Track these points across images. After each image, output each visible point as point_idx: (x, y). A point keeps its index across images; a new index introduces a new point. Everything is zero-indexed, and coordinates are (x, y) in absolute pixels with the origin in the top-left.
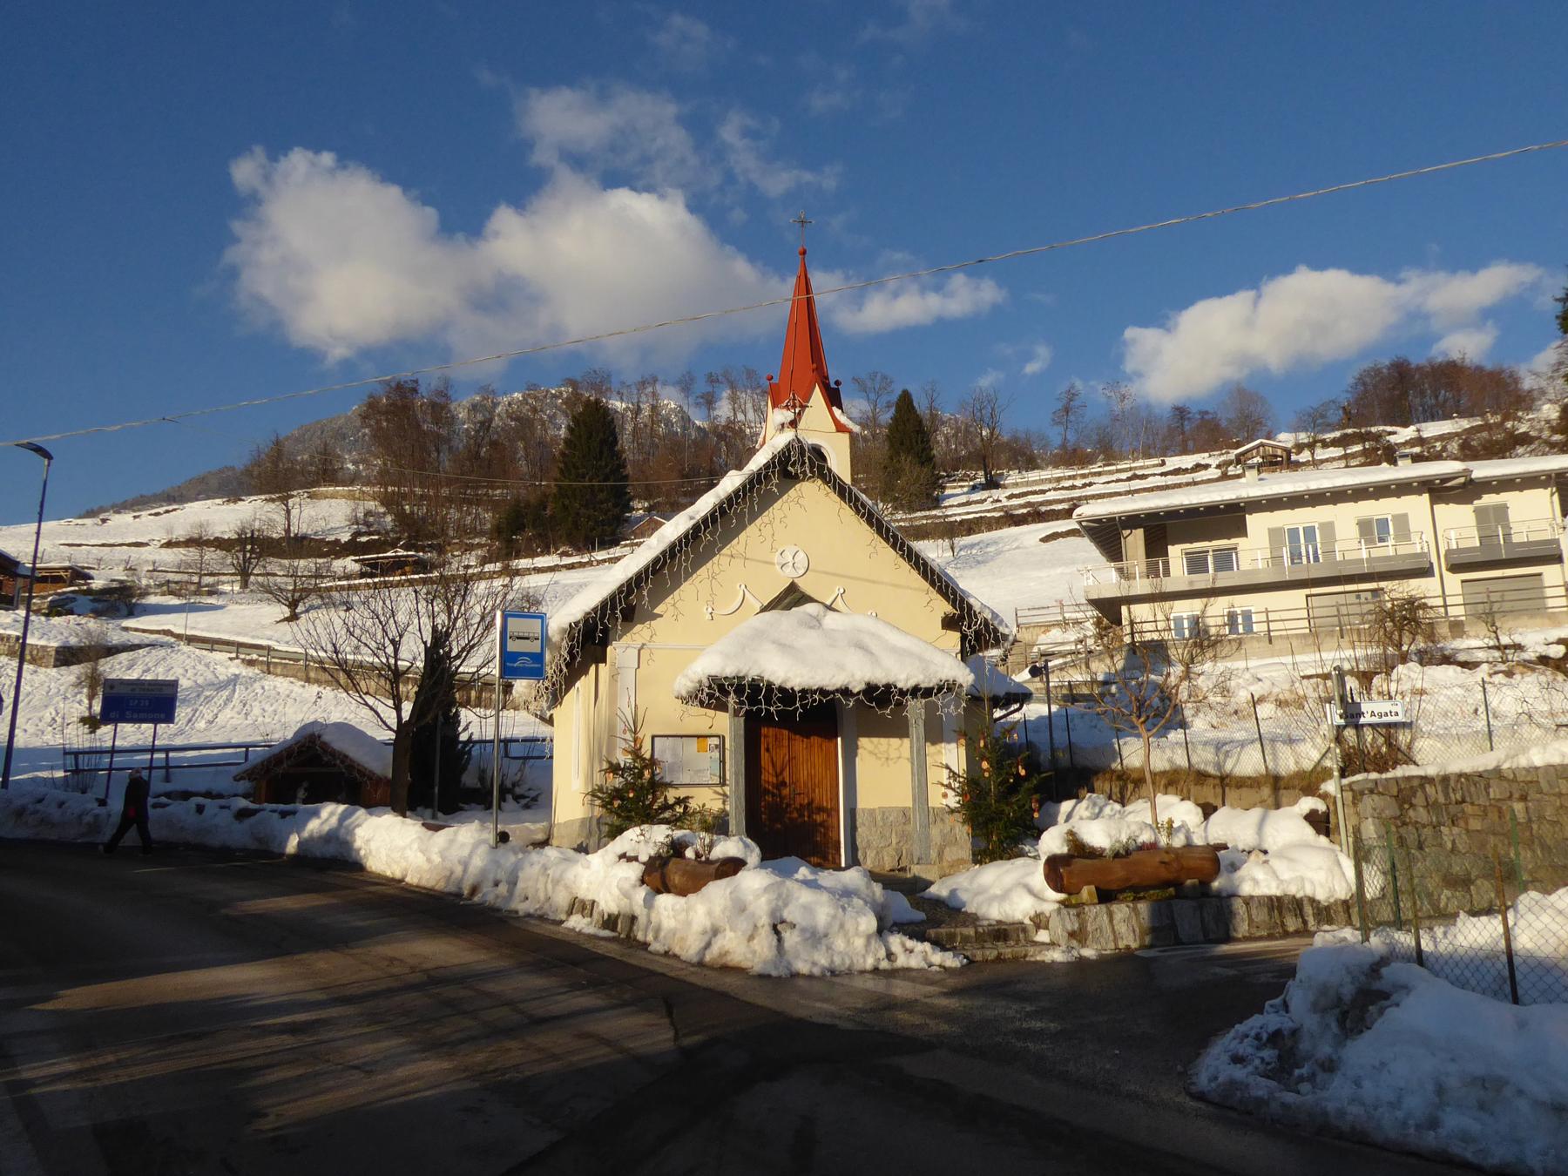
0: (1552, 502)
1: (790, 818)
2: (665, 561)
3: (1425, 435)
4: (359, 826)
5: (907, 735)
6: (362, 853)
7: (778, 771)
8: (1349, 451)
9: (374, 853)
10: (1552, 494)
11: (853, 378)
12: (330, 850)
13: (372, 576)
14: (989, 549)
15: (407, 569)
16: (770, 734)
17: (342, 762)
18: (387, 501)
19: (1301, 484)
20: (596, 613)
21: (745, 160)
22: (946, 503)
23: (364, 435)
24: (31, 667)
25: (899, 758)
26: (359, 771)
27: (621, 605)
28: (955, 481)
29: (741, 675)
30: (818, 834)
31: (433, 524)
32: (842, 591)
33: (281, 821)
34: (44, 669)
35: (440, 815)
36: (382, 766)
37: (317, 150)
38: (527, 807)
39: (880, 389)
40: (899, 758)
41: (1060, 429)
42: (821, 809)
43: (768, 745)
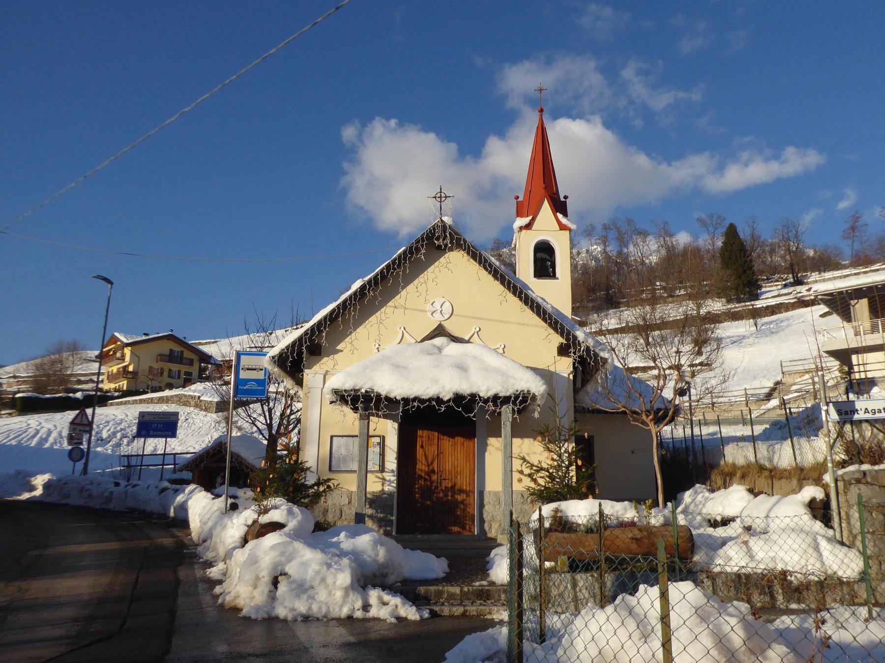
1: (437, 498)
5: (500, 436)
7: (430, 462)
14: (783, 324)
16: (424, 435)
20: (288, 350)
21: (639, 89)
22: (764, 296)
24: (204, 413)
27: (306, 342)
28: (772, 282)
29: (357, 388)
30: (459, 510)
32: (478, 329)
34: (210, 414)
37: (388, 119)
39: (716, 225)
41: (849, 242)
42: (461, 491)
43: (422, 443)
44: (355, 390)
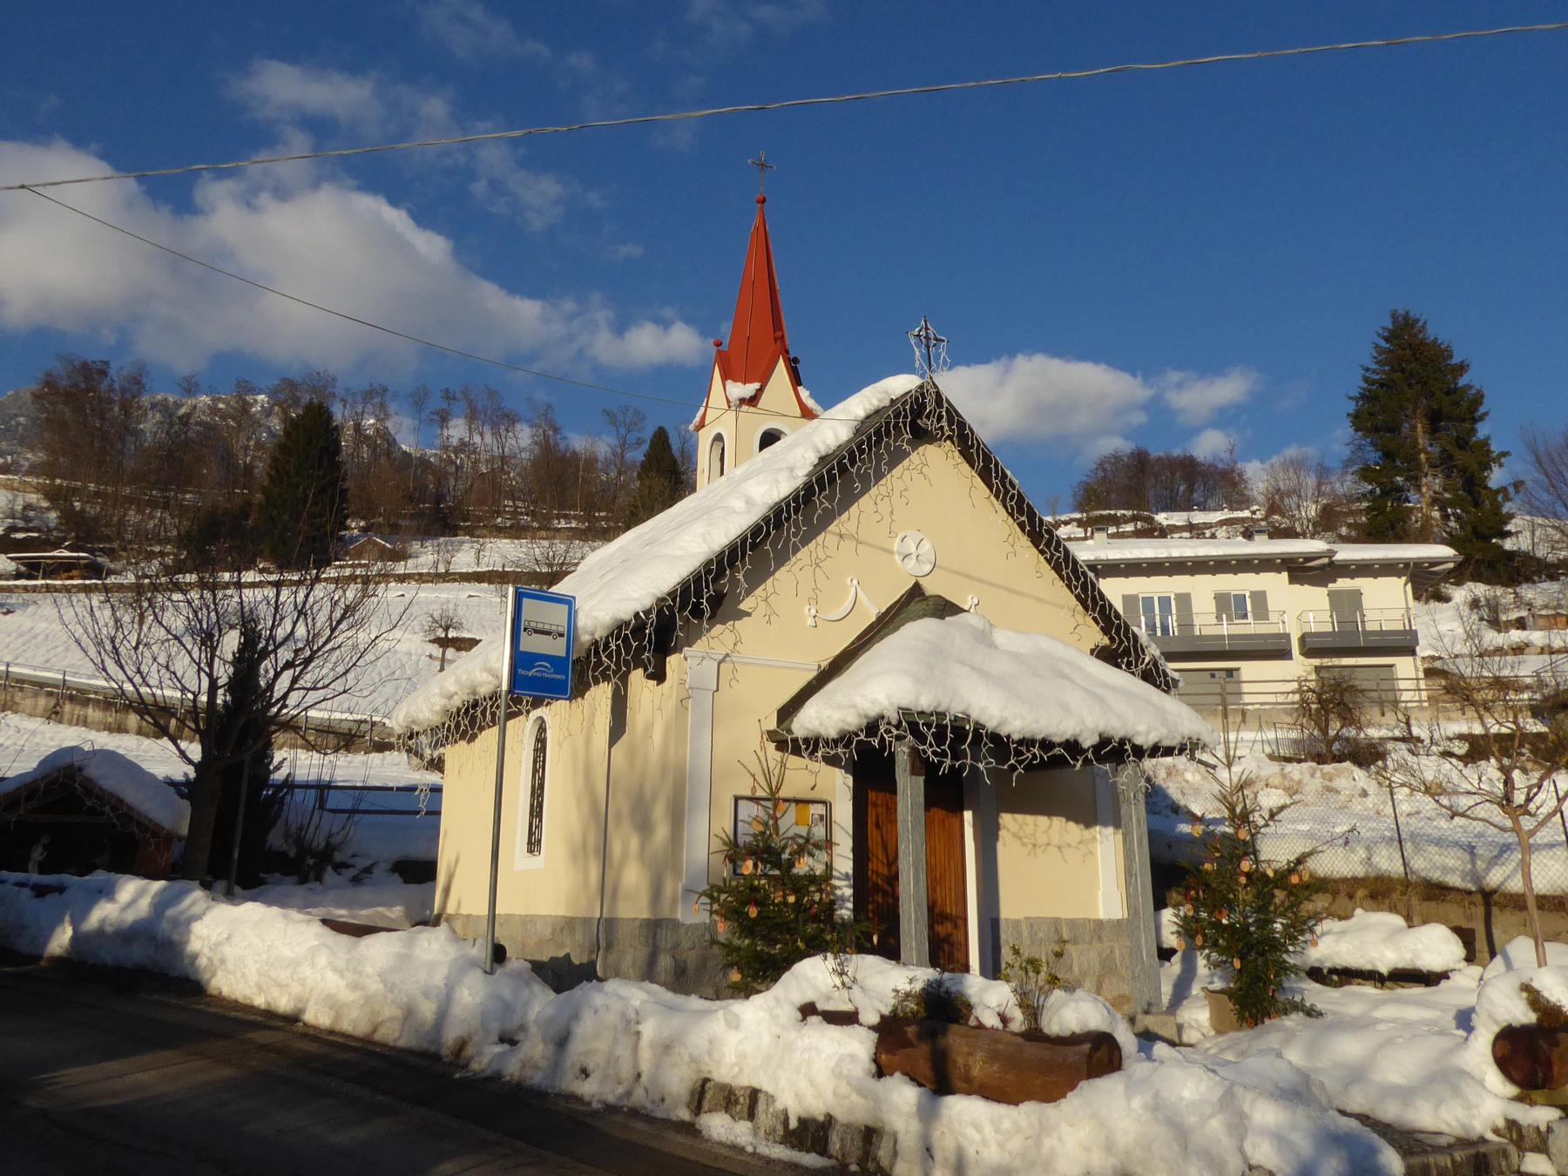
0: (1405, 592)
2: (768, 533)
3: (1195, 522)
4: (197, 918)
6: (203, 962)
8: (1121, 530)
9: (230, 965)
10: (1406, 585)
11: (604, 411)
12: (137, 954)
13: (29, 577)
15: (74, 573)
17: (114, 808)
18: (53, 495)
19: (1163, 550)
20: (674, 600)
23: (18, 424)
25: (1048, 844)
26: (139, 824)
31: (107, 525)
33: (36, 901)
35: (237, 889)
36: (178, 818)
38: (356, 881)
40: (1048, 844)
44: (938, 714)
